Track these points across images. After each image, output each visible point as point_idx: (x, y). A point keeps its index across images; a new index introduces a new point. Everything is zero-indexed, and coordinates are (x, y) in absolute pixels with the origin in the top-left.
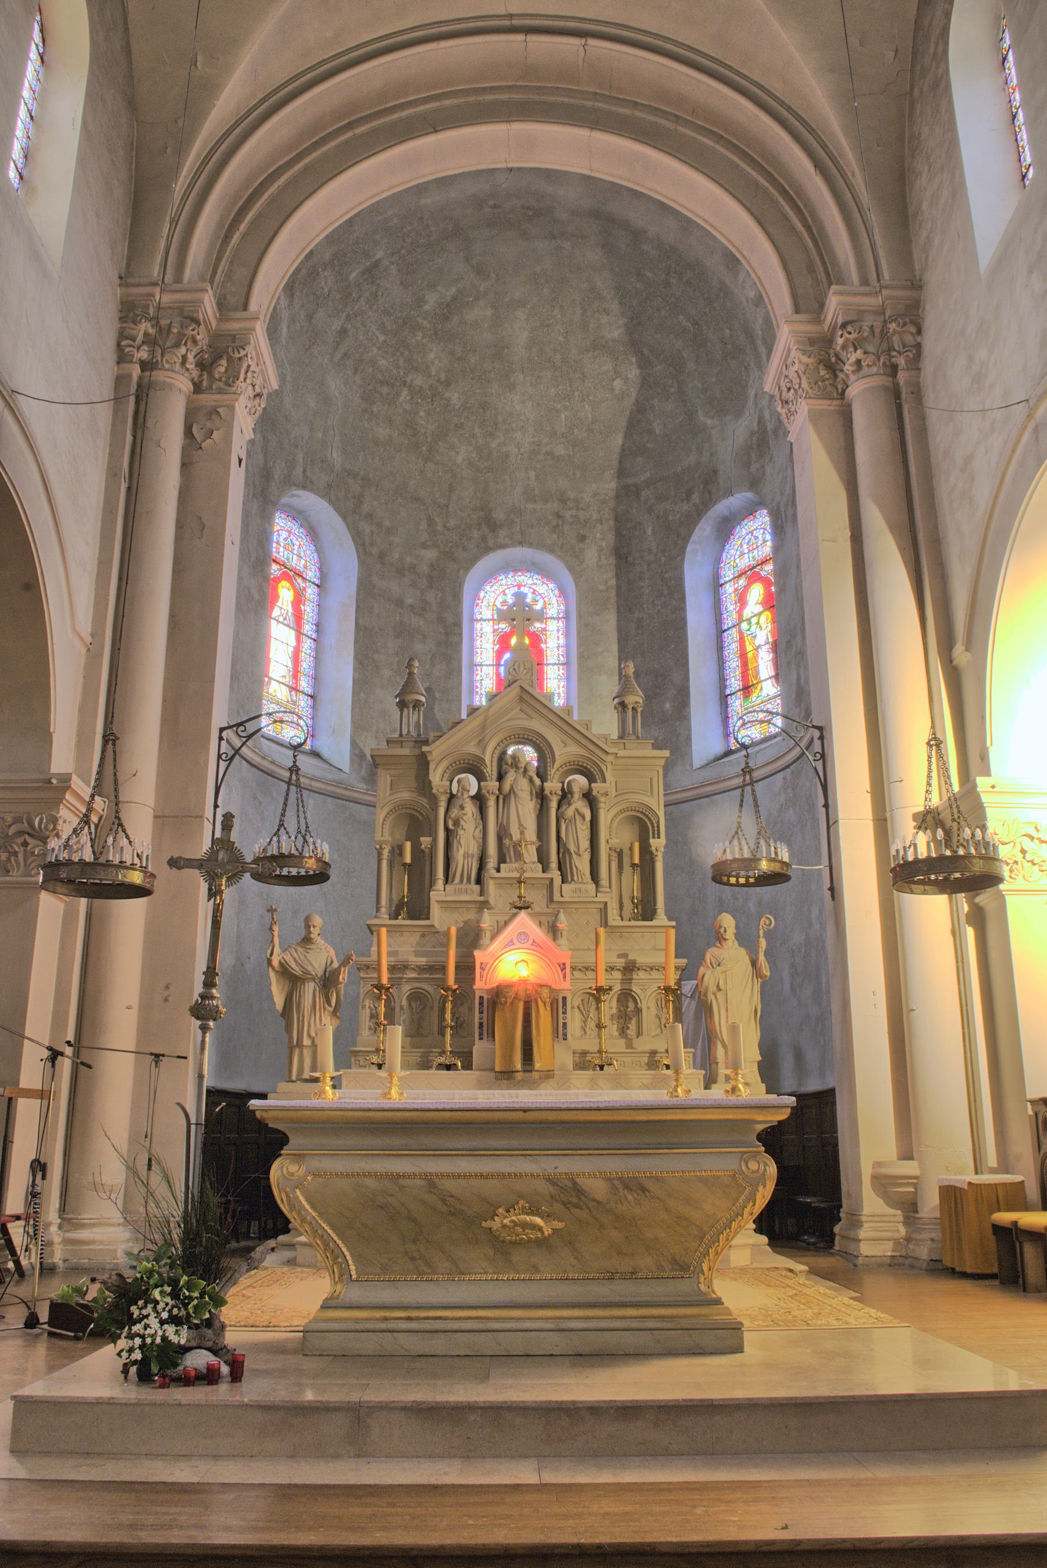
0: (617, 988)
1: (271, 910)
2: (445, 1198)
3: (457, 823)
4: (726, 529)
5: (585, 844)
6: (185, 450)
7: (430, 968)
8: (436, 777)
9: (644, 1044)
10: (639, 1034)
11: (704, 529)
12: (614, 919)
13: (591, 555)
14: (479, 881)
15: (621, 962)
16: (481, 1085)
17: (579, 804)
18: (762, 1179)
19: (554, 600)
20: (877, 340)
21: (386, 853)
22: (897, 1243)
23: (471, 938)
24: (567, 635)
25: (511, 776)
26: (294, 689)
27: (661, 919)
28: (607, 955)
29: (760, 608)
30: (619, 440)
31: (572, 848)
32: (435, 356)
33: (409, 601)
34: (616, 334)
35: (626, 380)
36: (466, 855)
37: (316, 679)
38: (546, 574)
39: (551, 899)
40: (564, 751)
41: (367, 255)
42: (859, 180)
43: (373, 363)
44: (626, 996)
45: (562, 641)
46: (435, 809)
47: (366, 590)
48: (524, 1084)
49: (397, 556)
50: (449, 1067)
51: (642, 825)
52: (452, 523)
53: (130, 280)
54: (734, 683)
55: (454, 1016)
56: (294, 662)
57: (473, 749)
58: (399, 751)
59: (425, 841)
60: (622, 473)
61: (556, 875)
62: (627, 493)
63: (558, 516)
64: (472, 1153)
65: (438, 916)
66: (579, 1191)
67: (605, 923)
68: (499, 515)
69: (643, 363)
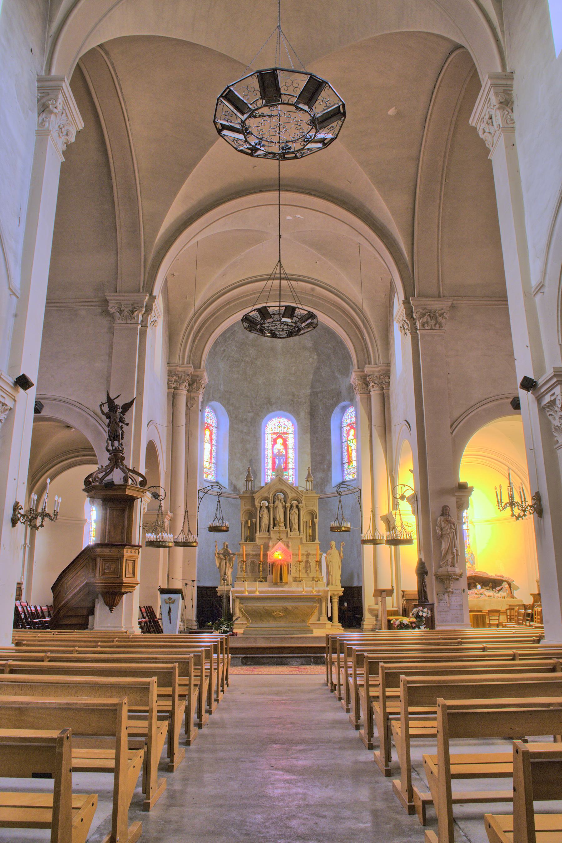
0: (305, 560)
1: (216, 542)
2: (266, 610)
3: (262, 515)
4: (344, 409)
5: (297, 521)
6: (186, 412)
7: (256, 555)
8: (256, 503)
9: (311, 575)
10: (310, 572)
11: (337, 410)
12: (304, 541)
13: (302, 414)
14: (268, 531)
15: (306, 553)
16: (270, 586)
17: (295, 510)
18: (316, 607)
19: (291, 427)
20: (378, 380)
21: (243, 523)
22: (373, 625)
23: (267, 548)
24: (295, 439)
25: (277, 502)
26: (211, 462)
27: (317, 541)
28: (302, 551)
29: (353, 438)
30: (311, 376)
31: (293, 522)
32: (252, 352)
33: (245, 431)
34: (310, 345)
35: (313, 359)
36: (265, 524)
37: (217, 459)
38: (289, 419)
39: (287, 536)
40: (291, 495)
41: (232, 330)
42: (375, 330)
43: (233, 357)
44: (307, 562)
45: (293, 441)
46: (257, 511)
47: (232, 429)
48: (280, 586)
49: (241, 416)
50: (261, 582)
51: (313, 515)
52: (258, 403)
53: (170, 365)
54: (346, 460)
55: (263, 569)
56: (211, 456)
57: (266, 495)
58: (246, 495)
59: (254, 520)
60: (312, 387)
61: (289, 530)
62: (314, 394)
63: (292, 401)
64: (270, 603)
65: (258, 541)
66: (287, 609)
67: (302, 543)
68: (273, 400)
69: (319, 355)
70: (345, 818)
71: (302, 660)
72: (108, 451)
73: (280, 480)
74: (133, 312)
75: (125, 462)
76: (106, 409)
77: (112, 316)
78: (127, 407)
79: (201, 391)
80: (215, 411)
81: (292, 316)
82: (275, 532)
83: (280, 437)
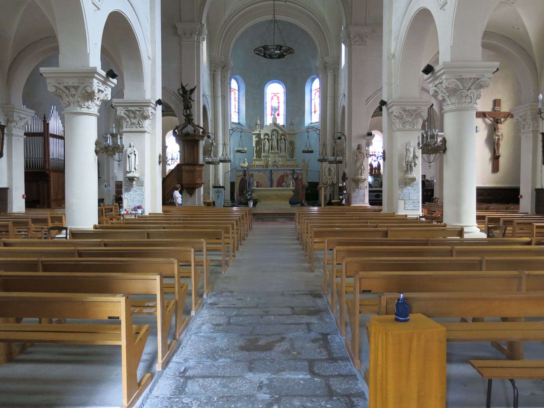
4: (313, 80)
11: (309, 80)
17: (283, 140)
40: (280, 132)
54: (313, 111)
56: (236, 109)
70: (306, 294)
71: (285, 219)
72: (184, 115)
73: (275, 124)
74: (191, 34)
75: (193, 121)
76: (181, 92)
77: (180, 36)
78: (192, 91)
79: (229, 72)
80: (237, 81)
81: (280, 50)
82: (271, 153)
83: (275, 95)
